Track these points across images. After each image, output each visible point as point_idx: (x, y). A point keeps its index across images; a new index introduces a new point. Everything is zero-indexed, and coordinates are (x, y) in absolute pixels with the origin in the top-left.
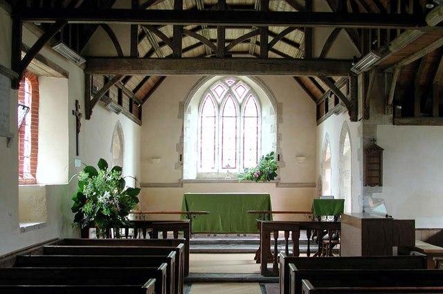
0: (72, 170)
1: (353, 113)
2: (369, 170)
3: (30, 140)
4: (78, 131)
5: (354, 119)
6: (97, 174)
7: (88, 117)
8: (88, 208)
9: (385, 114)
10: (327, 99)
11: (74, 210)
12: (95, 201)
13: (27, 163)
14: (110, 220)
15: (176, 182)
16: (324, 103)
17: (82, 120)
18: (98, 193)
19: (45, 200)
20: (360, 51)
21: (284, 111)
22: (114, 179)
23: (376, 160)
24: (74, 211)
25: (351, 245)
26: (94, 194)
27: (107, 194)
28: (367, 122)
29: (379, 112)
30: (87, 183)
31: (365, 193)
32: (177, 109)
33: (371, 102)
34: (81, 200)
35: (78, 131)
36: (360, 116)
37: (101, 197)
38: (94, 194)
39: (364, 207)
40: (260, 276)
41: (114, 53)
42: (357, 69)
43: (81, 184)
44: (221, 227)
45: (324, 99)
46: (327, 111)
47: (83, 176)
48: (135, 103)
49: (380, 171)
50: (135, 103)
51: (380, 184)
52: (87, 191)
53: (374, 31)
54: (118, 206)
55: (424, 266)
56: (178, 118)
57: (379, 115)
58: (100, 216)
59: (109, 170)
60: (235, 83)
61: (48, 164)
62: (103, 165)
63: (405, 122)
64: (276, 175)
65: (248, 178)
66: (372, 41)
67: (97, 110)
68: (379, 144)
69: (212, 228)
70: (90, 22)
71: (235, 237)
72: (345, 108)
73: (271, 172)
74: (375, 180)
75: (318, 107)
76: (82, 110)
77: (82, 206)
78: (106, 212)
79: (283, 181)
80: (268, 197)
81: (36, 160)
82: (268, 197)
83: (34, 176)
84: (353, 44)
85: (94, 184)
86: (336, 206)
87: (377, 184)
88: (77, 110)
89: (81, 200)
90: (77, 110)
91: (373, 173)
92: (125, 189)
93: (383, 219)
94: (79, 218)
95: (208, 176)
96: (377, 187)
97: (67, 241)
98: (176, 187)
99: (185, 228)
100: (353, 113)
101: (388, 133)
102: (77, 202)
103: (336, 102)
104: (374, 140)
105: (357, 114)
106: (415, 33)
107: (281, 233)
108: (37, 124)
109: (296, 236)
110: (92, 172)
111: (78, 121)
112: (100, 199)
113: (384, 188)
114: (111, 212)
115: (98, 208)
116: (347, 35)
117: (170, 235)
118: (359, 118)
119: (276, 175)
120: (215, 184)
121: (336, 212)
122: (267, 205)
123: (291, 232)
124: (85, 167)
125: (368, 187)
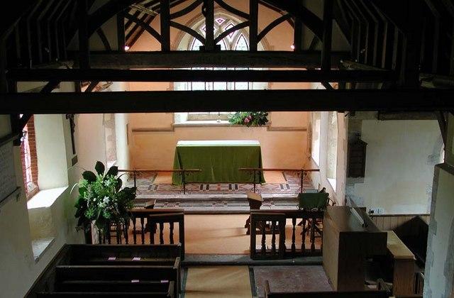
0: (72, 180)
3: (29, 152)
13: (28, 172)
19: (51, 219)
20: (350, 42)
26: (95, 200)
27: (106, 199)
31: (348, 184)
34: (82, 202)
35: (72, 131)
37: (101, 203)
38: (95, 200)
40: (250, 260)
41: (101, 47)
43: (82, 190)
47: (82, 182)
51: (363, 175)
52: (87, 197)
53: (361, 61)
59: (106, 172)
60: (225, 23)
61: (47, 189)
62: (100, 167)
64: (267, 121)
65: (239, 123)
66: (361, 50)
68: (363, 139)
70: (81, 282)
71: (225, 192)
78: (106, 215)
79: (273, 125)
80: (257, 151)
81: (36, 169)
83: (36, 183)
85: (94, 191)
86: (323, 196)
89: (82, 202)
91: (356, 164)
101: (371, 127)
104: (359, 135)
108: (34, 136)
110: (89, 177)
112: (101, 205)
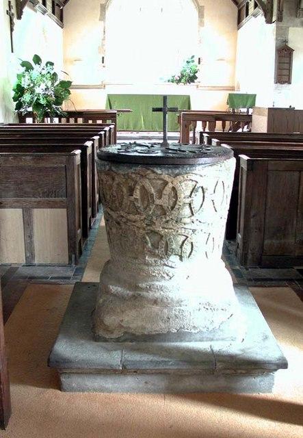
1: (269, 15)
2: (280, 69)
4: (12, 30)
5: (269, 21)
6: (33, 69)
7: (19, 17)
8: (27, 97)
10: (248, 3)
11: (15, 99)
12: (32, 92)
14: (45, 109)
15: (100, 83)
16: (245, 8)
17: (15, 20)
18: (35, 85)
21: (205, 15)
22: (49, 72)
23: (286, 60)
24: (15, 101)
25: (260, 125)
26: (32, 85)
28: (281, 24)
29: (291, 15)
30: (24, 76)
32: (98, 12)
33: (285, 5)
34: (20, 90)
35: (12, 30)
36: (274, 19)
44: (143, 126)
45: (245, 4)
46: (247, 14)
48: (57, 5)
50: (57, 5)
52: (25, 83)
54: (53, 96)
56: (100, 20)
57: (293, 18)
58: (37, 105)
62: (37, 60)
64: (196, 78)
67: (27, 10)
68: (290, 45)
69: (135, 126)
72: (261, 12)
73: (191, 75)
74: (285, 78)
75: (239, 12)
76: (14, 11)
77: (21, 96)
78: (43, 102)
79: (200, 85)
82: (188, 98)
87: (286, 82)
88: (10, 10)
90: (10, 10)
92: (58, 82)
93: (287, 109)
94: (19, 106)
97: (10, 125)
98: (99, 88)
99: (113, 117)
100: (269, 15)
102: (17, 93)
103: (256, 6)
104: (286, 41)
105: (272, 16)
107: (199, 124)
109: (213, 126)
111: (11, 20)
114: (47, 101)
115: (36, 98)
117: (99, 122)
118: (274, 20)
119: (196, 78)
120: (37, 245)
121: (248, 105)
122: (187, 102)
123: (208, 123)
124: (21, 62)
125: (279, 84)
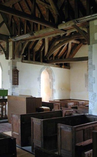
5: (7, 58)
9: (19, 58)
28: (14, 60)
36: (10, 58)
39: (12, 93)
42: (77, 21)
49: (18, 79)
53: (37, 24)
55: (62, 116)
57: (18, 58)
63: (26, 62)
68: (17, 69)
84: (7, 30)
93: (30, 98)
95: (53, 3)
96: (16, 85)
100: (7, 56)
101: (20, 65)
104: (16, 67)
106: (51, 30)
113: (19, 86)
116: (6, 26)
125: (14, 85)
